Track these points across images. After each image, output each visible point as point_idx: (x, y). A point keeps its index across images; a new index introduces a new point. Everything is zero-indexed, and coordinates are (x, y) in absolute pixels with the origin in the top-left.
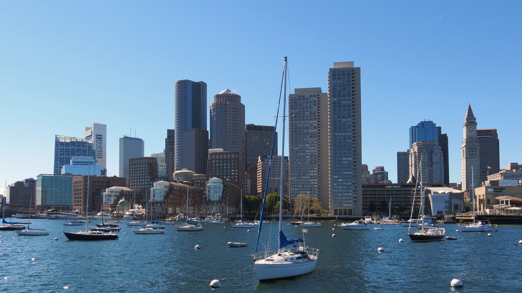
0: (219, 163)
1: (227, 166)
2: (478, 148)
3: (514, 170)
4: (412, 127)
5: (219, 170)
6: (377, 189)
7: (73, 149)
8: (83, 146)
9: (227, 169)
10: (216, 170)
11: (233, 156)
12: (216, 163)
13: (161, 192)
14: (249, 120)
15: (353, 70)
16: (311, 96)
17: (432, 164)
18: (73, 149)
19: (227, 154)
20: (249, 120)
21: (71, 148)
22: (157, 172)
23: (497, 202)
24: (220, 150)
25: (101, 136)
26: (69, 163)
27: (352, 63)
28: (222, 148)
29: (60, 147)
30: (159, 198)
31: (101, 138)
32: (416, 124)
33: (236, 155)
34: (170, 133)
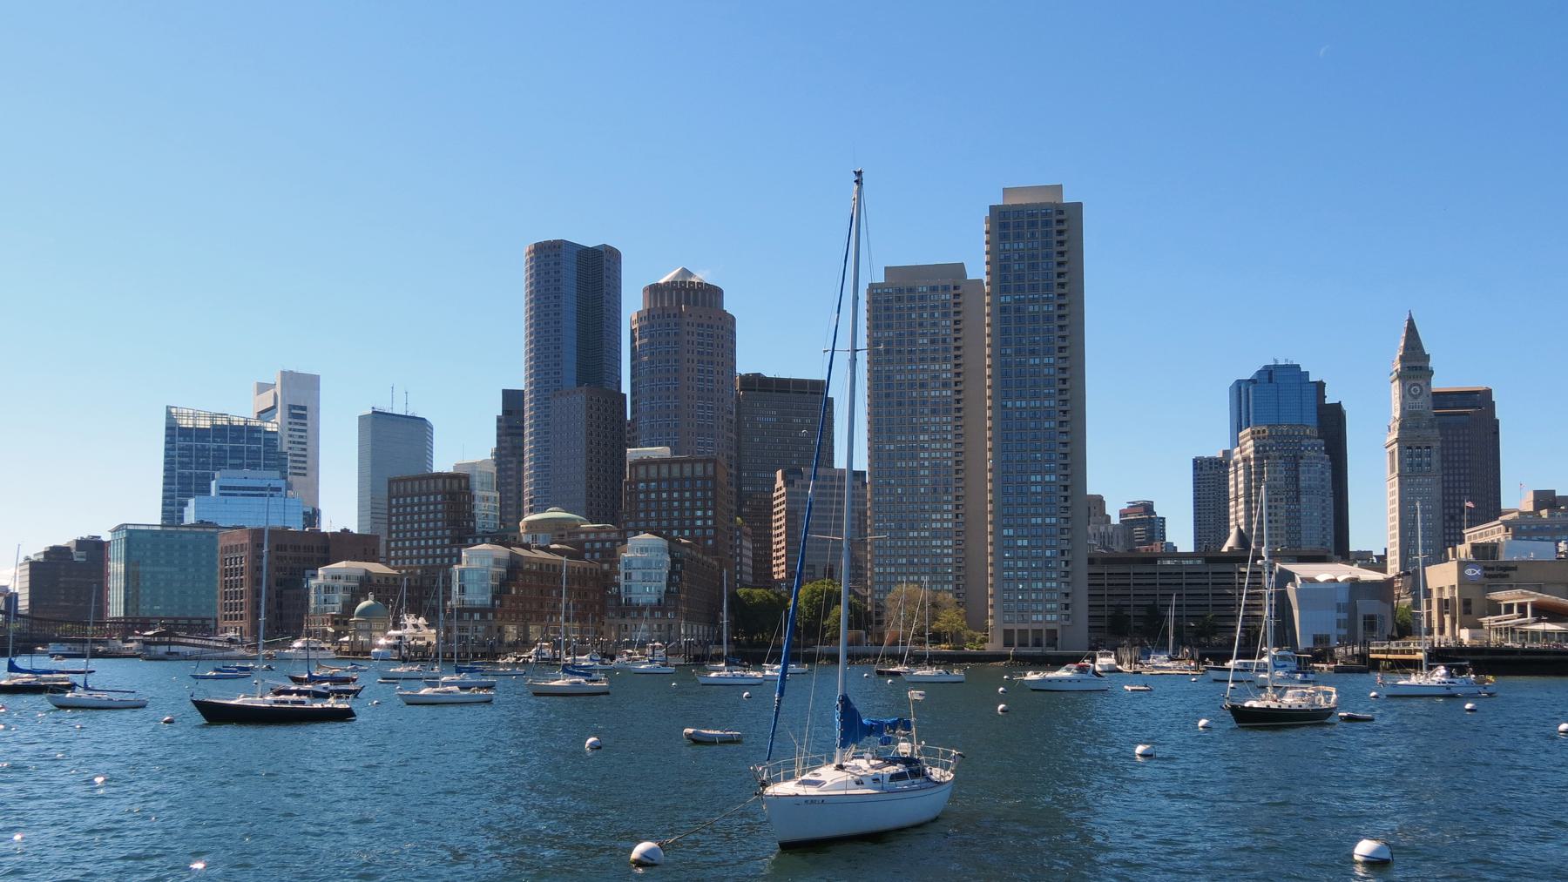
0: (659, 492)
1: (682, 500)
2: (1436, 445)
3: (1544, 513)
4: (1239, 382)
5: (659, 512)
6: (1133, 569)
7: (220, 449)
8: (251, 440)
9: (681, 509)
10: (647, 512)
11: (699, 468)
12: (648, 492)
13: (483, 578)
14: (748, 362)
15: (1061, 209)
16: (934, 289)
17: (1298, 492)
18: (220, 449)
19: (681, 462)
20: (748, 362)
21: (214, 445)
22: (472, 517)
23: (1494, 609)
24: (662, 451)
25: (304, 408)
26: (209, 491)
27: (1058, 189)
28: (667, 444)
29: (180, 442)
30: (478, 595)
31: (303, 417)
32: (1248, 374)
33: (710, 468)
34: (512, 399)
